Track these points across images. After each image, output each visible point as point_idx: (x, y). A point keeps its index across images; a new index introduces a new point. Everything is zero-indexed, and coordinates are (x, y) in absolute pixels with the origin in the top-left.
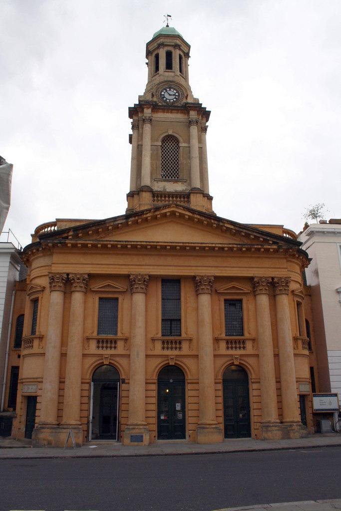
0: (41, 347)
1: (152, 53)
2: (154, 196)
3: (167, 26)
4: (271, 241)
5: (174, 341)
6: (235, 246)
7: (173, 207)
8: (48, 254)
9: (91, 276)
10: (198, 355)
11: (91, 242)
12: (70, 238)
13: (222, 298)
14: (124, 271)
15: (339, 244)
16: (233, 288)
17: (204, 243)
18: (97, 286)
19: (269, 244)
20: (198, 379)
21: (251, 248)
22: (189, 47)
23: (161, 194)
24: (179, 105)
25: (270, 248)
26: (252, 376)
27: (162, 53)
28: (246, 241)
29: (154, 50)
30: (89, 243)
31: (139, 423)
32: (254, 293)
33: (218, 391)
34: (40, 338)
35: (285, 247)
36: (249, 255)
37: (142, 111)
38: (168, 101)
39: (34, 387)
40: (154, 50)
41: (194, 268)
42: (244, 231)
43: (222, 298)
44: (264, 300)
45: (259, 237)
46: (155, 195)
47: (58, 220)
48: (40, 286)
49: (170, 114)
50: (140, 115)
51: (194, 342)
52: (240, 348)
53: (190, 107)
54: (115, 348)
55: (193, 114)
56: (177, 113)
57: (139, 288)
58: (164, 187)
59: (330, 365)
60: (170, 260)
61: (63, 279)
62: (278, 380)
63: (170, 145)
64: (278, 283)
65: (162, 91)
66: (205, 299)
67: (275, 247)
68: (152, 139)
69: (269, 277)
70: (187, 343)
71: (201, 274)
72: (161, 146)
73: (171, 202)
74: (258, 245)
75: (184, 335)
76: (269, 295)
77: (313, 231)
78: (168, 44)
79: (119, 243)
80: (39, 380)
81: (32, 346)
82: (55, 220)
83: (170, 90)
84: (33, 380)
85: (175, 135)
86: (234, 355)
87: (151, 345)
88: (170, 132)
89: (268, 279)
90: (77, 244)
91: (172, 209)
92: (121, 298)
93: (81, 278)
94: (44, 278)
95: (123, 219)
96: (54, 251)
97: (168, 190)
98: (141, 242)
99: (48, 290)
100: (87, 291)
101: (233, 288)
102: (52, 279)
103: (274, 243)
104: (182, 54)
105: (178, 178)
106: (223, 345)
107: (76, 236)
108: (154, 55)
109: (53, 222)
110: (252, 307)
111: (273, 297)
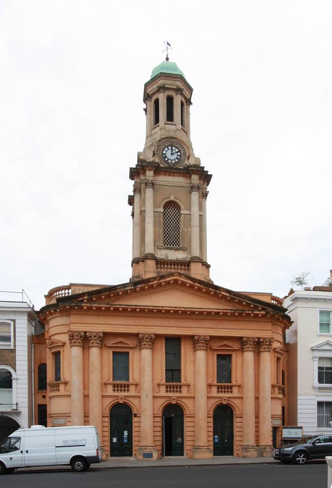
0: (66, 390)
1: (151, 98)
2: (157, 264)
6: (230, 311)
7: (176, 275)
11: (105, 306)
13: (215, 354)
14: (134, 330)
18: (111, 342)
27: (162, 98)
28: (239, 307)
31: (202, 445)
32: (242, 350)
38: (170, 161)
40: (153, 94)
41: (193, 329)
42: (238, 298)
43: (215, 354)
44: (249, 356)
45: (250, 304)
46: (160, 263)
47: (72, 285)
50: (142, 177)
51: (192, 388)
52: (228, 392)
55: (195, 178)
56: (179, 176)
61: (81, 337)
63: (171, 211)
65: (164, 150)
67: (263, 312)
68: (155, 205)
75: (62, 379)
76: (254, 351)
78: (170, 86)
81: (59, 390)
82: (68, 284)
87: (157, 389)
88: (172, 198)
92: (61, 350)
96: (72, 312)
99: (68, 345)
102: (72, 337)
103: (263, 309)
105: (179, 246)
107: (90, 300)
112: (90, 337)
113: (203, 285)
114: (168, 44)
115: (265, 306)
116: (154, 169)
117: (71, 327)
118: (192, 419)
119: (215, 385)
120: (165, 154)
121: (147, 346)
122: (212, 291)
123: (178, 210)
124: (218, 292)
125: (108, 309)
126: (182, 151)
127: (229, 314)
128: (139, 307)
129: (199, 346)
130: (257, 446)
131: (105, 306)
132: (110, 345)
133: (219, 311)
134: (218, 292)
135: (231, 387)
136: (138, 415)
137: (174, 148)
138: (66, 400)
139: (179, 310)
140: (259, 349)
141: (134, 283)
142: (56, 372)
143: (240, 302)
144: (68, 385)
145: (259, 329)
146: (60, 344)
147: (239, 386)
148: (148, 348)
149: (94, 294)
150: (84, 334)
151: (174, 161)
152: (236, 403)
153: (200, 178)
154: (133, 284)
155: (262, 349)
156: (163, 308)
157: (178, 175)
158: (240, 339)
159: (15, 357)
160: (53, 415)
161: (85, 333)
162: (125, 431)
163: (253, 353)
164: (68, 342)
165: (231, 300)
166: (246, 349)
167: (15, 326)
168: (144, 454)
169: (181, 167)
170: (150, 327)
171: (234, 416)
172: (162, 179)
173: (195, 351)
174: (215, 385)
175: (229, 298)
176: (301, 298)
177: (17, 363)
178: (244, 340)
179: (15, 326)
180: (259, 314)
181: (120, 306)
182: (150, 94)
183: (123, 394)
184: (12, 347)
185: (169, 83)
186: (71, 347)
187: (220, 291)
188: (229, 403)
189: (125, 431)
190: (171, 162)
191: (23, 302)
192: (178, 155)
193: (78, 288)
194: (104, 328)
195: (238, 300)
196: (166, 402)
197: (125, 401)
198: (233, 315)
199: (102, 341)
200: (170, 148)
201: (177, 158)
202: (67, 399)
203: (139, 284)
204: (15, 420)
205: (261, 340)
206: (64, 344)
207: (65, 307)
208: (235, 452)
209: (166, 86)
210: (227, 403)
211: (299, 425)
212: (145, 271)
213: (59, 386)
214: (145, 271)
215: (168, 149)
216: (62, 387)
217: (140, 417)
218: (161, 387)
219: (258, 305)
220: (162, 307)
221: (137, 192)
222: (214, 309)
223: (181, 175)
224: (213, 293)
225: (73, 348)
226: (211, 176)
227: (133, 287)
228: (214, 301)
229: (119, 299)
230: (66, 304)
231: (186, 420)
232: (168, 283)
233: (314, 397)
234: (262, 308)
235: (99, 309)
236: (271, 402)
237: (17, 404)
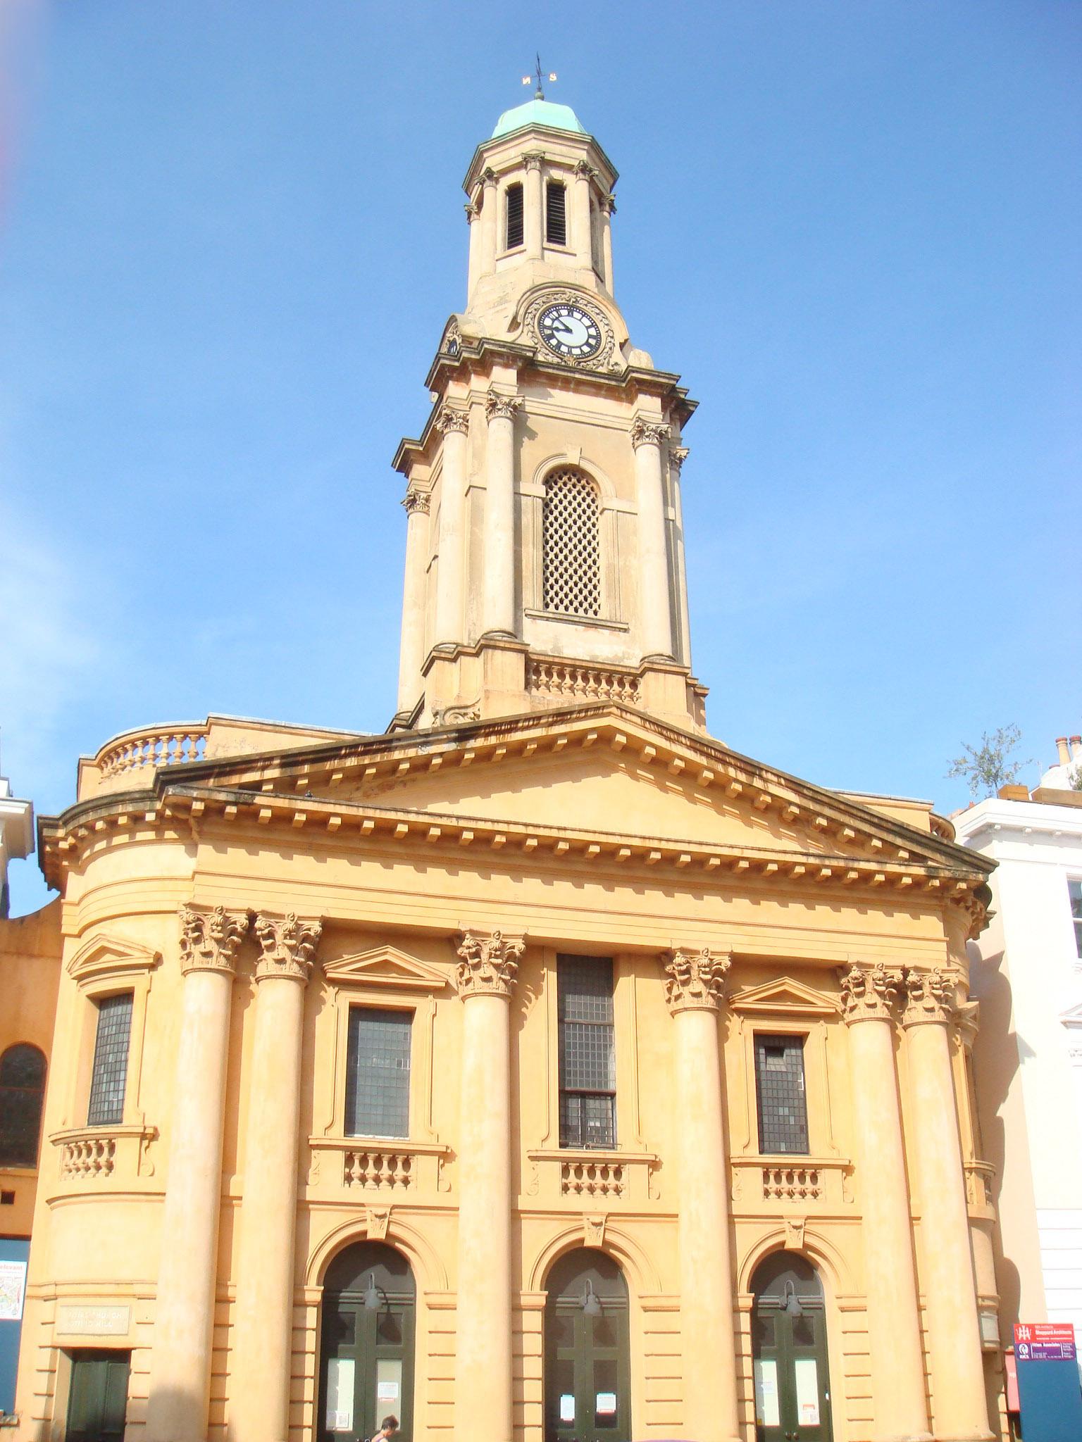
0: (146, 1170)
1: (497, 181)
4: (905, 849)
12: (265, 788)
18: (750, 994)
19: (904, 862)
23: (551, 664)
29: (505, 172)
34: (143, 1136)
35: (947, 874)
38: (564, 349)
40: (505, 172)
41: (667, 923)
42: (828, 812)
45: (870, 836)
46: (534, 668)
48: (144, 950)
53: (492, 353)
61: (233, 932)
63: (566, 494)
67: (919, 871)
72: (543, 499)
73: (604, 698)
74: (868, 861)
77: (991, 826)
78: (558, 159)
79: (827, 862)
80: (139, 1289)
81: (110, 1167)
83: (570, 314)
84: (356, 1301)
85: (585, 465)
88: (572, 458)
90: (293, 812)
92: (423, 1006)
95: (449, 741)
98: (508, 823)
103: (915, 858)
105: (595, 613)
107: (286, 786)
113: (702, 753)
115: (919, 844)
116: (520, 364)
121: (479, 985)
122: (736, 781)
123: (592, 496)
124: (758, 783)
126: (601, 325)
128: (472, 824)
132: (342, 973)
134: (758, 783)
141: (458, 731)
142: (95, 1085)
143: (831, 831)
148: (485, 994)
149: (303, 763)
151: (576, 351)
153: (664, 408)
156: (562, 834)
157: (594, 390)
158: (831, 973)
163: (947, 1029)
164: (172, 953)
165: (801, 823)
169: (601, 370)
175: (796, 810)
180: (901, 876)
181: (401, 816)
182: (495, 169)
186: (185, 973)
187: (766, 781)
190: (570, 352)
192: (590, 336)
199: (310, 956)
201: (587, 344)
202: (145, 1207)
205: (913, 977)
206: (155, 963)
207: (188, 808)
212: (487, 691)
213: (112, 1148)
214: (487, 691)
216: (126, 1150)
220: (559, 829)
222: (747, 848)
223: (603, 392)
224: (739, 787)
227: (451, 747)
229: (391, 787)
230: (195, 794)
232: (518, 750)
234: (911, 852)
235: (318, 822)
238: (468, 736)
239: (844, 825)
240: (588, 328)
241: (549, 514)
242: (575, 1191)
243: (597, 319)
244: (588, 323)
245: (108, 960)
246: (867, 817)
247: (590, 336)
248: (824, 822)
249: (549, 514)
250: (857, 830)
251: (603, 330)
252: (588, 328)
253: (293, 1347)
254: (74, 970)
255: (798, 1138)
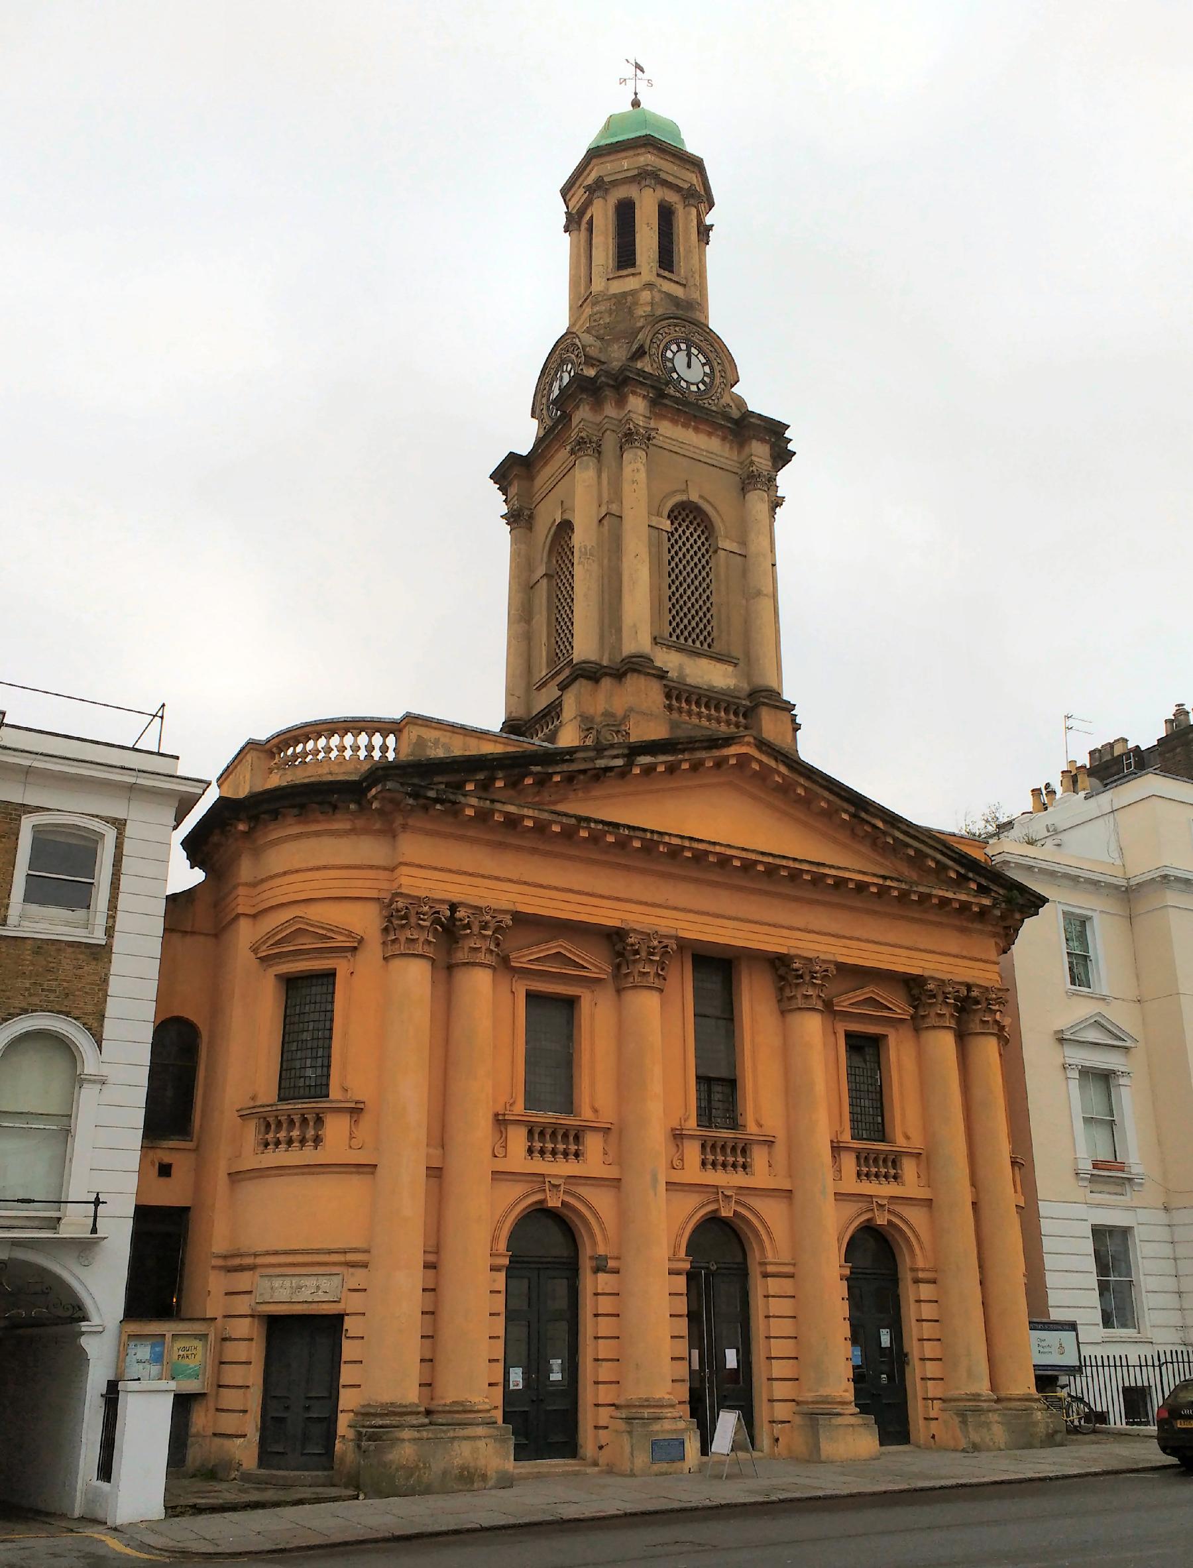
1: (607, 191)
2: (668, 696)
3: (636, 104)
5: (549, 1131)
6: (876, 880)
7: (748, 744)
8: (378, 826)
9: (522, 920)
10: (440, 1169)
11: (536, 814)
13: (841, 1028)
14: (608, 916)
15: (1061, 908)
16: (871, 1002)
17: (823, 865)
20: (367, 1251)
21: (492, 812)
22: (697, 165)
23: (690, 694)
24: (714, 408)
25: (950, 900)
26: (598, 1243)
27: (603, 214)
28: (911, 874)
29: (614, 183)
30: (529, 815)
32: (917, 1025)
33: (1148, 1277)
36: (917, 915)
37: (621, 402)
38: (683, 384)
39: (324, 1283)
43: (841, 1028)
44: (944, 1043)
47: (412, 719)
49: (690, 430)
50: (610, 410)
52: (566, 1154)
54: (317, 1140)
55: (760, 452)
56: (710, 434)
57: (799, 996)
58: (681, 667)
59: (1044, 1223)
60: (725, 902)
62: (431, 1258)
64: (468, 926)
65: (667, 348)
66: (811, 1026)
67: (987, 902)
69: (442, 901)
70: (765, 1149)
71: (805, 955)
75: (335, 1093)
76: (433, 961)
78: (670, 179)
82: (397, 715)
86: (549, 1175)
88: (694, 497)
89: (438, 907)
91: (744, 750)
92: (342, 967)
93: (492, 925)
94: (358, 907)
96: (411, 822)
97: (689, 681)
99: (373, 949)
100: (504, 965)
101: (871, 1002)
104: (672, 197)
105: (709, 646)
106: (518, 1139)
108: (584, 225)
109: (394, 722)
110: (909, 1064)
111: (962, 1037)
112: (468, 926)
114: (638, 67)
117: (404, 881)
118: (786, 1286)
119: (692, 1137)
120: (672, 360)
125: (541, 828)
127: (712, 859)
129: (806, 997)
130: (998, 1401)
131: (536, 814)
133: (847, 875)
135: (894, 1160)
136: (611, 1264)
137: (694, 351)
138: (355, 1185)
139: (756, 862)
140: (450, 952)
144: (366, 1120)
145: (964, 953)
146: (340, 941)
147: (607, 1131)
150: (448, 913)
152: (912, 1221)
154: (626, 751)
155: (461, 956)
158: (913, 985)
159: (105, 981)
160: (259, 1260)
161: (453, 907)
162: (888, 1345)
166: (932, 1021)
167: (119, 846)
168: (654, 1443)
170: (659, 911)
171: (906, 1277)
172: (668, 430)
173: (450, 968)
174: (692, 1137)
176: (1177, 879)
177: (112, 1008)
178: (630, 940)
179: (119, 846)
182: (606, 179)
183: (563, 1168)
184: (99, 937)
185: (669, 169)
188: (743, 1218)
189: (888, 1345)
190: (688, 387)
191: (134, 749)
192: (705, 374)
193: (430, 734)
194: (519, 898)
195: (916, 850)
196: (526, 1196)
197: (740, 1210)
198: (883, 891)
200: (683, 346)
201: (703, 382)
203: (645, 754)
204: (66, 1275)
208: (588, 1439)
209: (663, 176)
210: (889, 1221)
211: (1055, 1315)
215: (679, 349)
217: (617, 1271)
218: (687, 1143)
219: (971, 875)
221: (590, 452)
225: (396, 964)
226: (491, 477)
228: (835, 841)
231: (759, 1287)
233: (1080, 1210)
236: (668, 1201)
237: (97, 1202)
238: (884, 821)
239: (927, 856)
240: (704, 365)
241: (1059, 790)
242: (711, 1167)
243: (712, 356)
244: (704, 361)
245: (308, 943)
246: (950, 853)
247: (705, 374)
248: (912, 853)
249: (1059, 790)
250: (938, 862)
251: (717, 368)
252: (704, 365)
253: (435, 1321)
254: (261, 950)
255: (880, 1132)
